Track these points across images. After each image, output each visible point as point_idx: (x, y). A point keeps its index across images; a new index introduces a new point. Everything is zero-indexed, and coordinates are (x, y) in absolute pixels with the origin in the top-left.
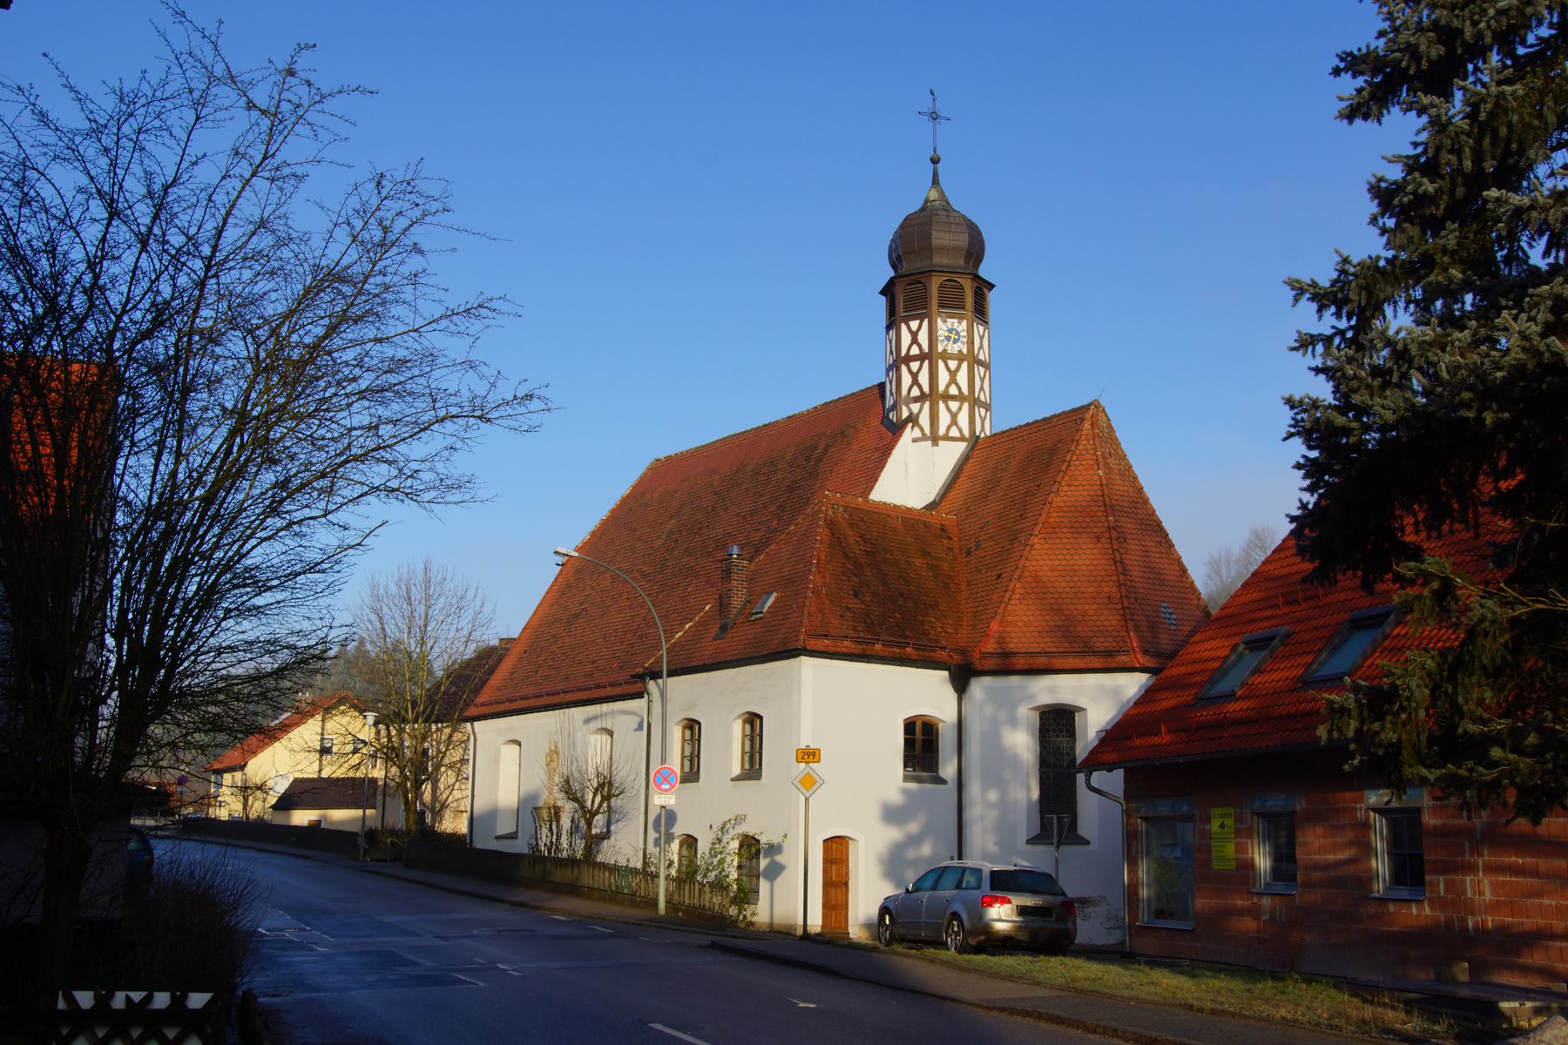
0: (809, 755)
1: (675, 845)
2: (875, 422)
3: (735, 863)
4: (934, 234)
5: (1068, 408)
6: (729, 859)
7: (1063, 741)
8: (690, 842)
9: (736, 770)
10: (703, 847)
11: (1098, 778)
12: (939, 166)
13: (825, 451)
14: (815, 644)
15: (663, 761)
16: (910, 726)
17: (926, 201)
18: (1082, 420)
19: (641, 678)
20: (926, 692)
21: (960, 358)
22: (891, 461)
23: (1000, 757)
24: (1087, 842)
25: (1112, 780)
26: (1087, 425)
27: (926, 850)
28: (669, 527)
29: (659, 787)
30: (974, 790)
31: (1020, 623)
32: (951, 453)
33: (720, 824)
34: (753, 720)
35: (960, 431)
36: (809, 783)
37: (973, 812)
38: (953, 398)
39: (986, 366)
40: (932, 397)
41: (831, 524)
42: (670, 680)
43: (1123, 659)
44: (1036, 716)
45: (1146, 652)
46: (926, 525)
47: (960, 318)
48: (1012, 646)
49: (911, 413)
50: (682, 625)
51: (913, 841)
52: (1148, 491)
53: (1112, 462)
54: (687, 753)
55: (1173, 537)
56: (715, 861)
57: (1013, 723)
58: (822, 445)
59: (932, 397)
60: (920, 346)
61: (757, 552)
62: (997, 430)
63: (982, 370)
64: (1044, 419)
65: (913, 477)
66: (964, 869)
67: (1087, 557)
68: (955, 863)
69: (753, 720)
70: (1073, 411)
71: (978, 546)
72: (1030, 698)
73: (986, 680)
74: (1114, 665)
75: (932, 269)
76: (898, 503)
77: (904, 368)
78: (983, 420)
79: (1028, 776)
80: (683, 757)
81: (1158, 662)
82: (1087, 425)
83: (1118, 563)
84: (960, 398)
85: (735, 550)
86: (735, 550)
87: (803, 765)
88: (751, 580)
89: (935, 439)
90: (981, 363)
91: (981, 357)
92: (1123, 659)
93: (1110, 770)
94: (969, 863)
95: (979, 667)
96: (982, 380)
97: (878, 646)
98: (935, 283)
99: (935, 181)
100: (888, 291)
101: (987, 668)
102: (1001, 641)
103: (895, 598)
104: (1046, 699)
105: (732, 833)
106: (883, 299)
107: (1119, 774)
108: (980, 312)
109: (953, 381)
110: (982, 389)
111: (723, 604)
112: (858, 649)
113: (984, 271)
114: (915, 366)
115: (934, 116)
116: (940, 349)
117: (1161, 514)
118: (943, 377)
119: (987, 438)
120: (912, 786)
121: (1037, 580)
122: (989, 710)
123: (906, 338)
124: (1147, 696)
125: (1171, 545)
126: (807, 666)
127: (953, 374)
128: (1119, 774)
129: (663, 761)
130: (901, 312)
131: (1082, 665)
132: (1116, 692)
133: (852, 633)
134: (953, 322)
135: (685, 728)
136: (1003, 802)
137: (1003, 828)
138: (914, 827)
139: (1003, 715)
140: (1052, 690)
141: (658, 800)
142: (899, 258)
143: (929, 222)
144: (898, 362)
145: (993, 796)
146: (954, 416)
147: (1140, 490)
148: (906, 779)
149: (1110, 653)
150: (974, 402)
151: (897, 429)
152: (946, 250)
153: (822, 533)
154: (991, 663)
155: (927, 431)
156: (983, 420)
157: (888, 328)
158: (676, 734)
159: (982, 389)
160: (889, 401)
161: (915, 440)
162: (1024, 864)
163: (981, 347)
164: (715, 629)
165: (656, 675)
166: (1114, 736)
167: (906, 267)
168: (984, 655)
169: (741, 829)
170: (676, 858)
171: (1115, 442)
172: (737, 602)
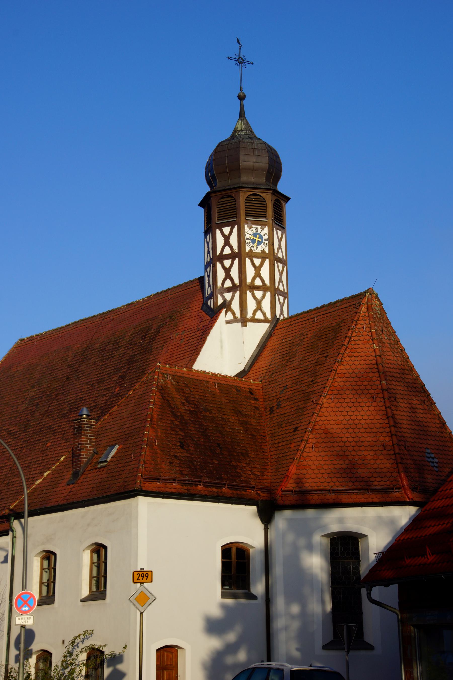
0: (143, 576)
1: (33, 661)
2: (197, 307)
3: (83, 673)
4: (241, 157)
5: (348, 295)
6: (78, 669)
7: (246, 370)
8: (45, 656)
9: (85, 592)
10: (57, 660)
11: (376, 592)
12: (245, 102)
13: (158, 332)
14: (148, 486)
15: (24, 587)
16: (226, 551)
17: (235, 131)
18: (360, 304)
19: (7, 518)
20: (240, 524)
21: (263, 256)
22: (209, 338)
23: (299, 577)
24: (371, 648)
25: (388, 594)
26: (364, 309)
27: (242, 656)
28: (31, 394)
29: (19, 609)
30: (279, 603)
31: (313, 466)
32: (257, 332)
33: (71, 639)
34: (99, 550)
35: (264, 314)
36: (144, 600)
37: (279, 623)
38: (258, 288)
39: (284, 262)
40: (241, 287)
41: (162, 390)
42: (31, 519)
43: (396, 495)
44: (326, 542)
45: (413, 489)
46: (238, 390)
47: (263, 225)
48: (307, 485)
49: (225, 300)
50: (42, 473)
51: (231, 649)
52: (413, 360)
53: (384, 337)
54: (45, 579)
55: (434, 396)
56: (67, 671)
57: (310, 548)
58: (155, 326)
59: (241, 287)
60: (231, 247)
61: (103, 413)
62: (293, 313)
63: (281, 266)
64: (330, 304)
65: (227, 351)
66: (270, 669)
67: (366, 413)
68: (265, 664)
69: (99, 550)
70: (353, 297)
71: (279, 406)
72: (324, 527)
73: (288, 513)
74: (389, 500)
75: (240, 185)
76: (216, 372)
77: (219, 265)
78: (282, 306)
79: (322, 592)
80: (41, 583)
81: (422, 495)
82: (364, 309)
83: (390, 418)
84: (263, 288)
85: (85, 411)
86: (85, 411)
87: (139, 585)
88: (97, 435)
89: (244, 321)
90: (280, 260)
91: (280, 255)
92: (396, 495)
93: (386, 586)
94: (274, 664)
95: (281, 502)
96: (281, 274)
97: (200, 487)
98: (243, 196)
99: (242, 115)
100: (205, 203)
101: (287, 503)
102: (299, 481)
103: (211, 446)
104: (335, 528)
105: (81, 646)
106: (202, 210)
107: (394, 588)
108: (279, 220)
109: (258, 274)
110: (281, 281)
111: (75, 456)
112: (184, 489)
113: (281, 187)
114: (227, 263)
115: (240, 61)
116: (247, 249)
117: (424, 378)
118: (250, 272)
119: (285, 319)
120: (229, 601)
121: (326, 432)
122: (290, 538)
123: (220, 241)
124: (415, 523)
125: (432, 403)
126: (143, 502)
127: (258, 269)
128: (394, 588)
129: (24, 587)
130: (216, 220)
131: (363, 500)
132: (392, 522)
133: (178, 477)
134: (257, 228)
135: (43, 558)
136: (304, 615)
137: (304, 635)
138: (231, 637)
139: (302, 542)
140: (341, 520)
141: (18, 621)
142: (213, 177)
143: (238, 148)
144: (211, 264)
145: (295, 609)
146: (259, 303)
147: (407, 359)
148: (224, 595)
149: (386, 490)
150: (275, 292)
151: (214, 314)
152: (251, 170)
153: (154, 396)
154: (291, 499)
155: (238, 315)
156: (282, 306)
157: (206, 233)
158: (36, 564)
159: (281, 281)
160: (208, 291)
161: (228, 322)
162: (318, 665)
163: (280, 247)
164: (69, 475)
165: (19, 516)
166: (388, 556)
167: (219, 185)
168: (286, 493)
169: (89, 643)
170: (33, 671)
171: (385, 321)
172: (86, 453)
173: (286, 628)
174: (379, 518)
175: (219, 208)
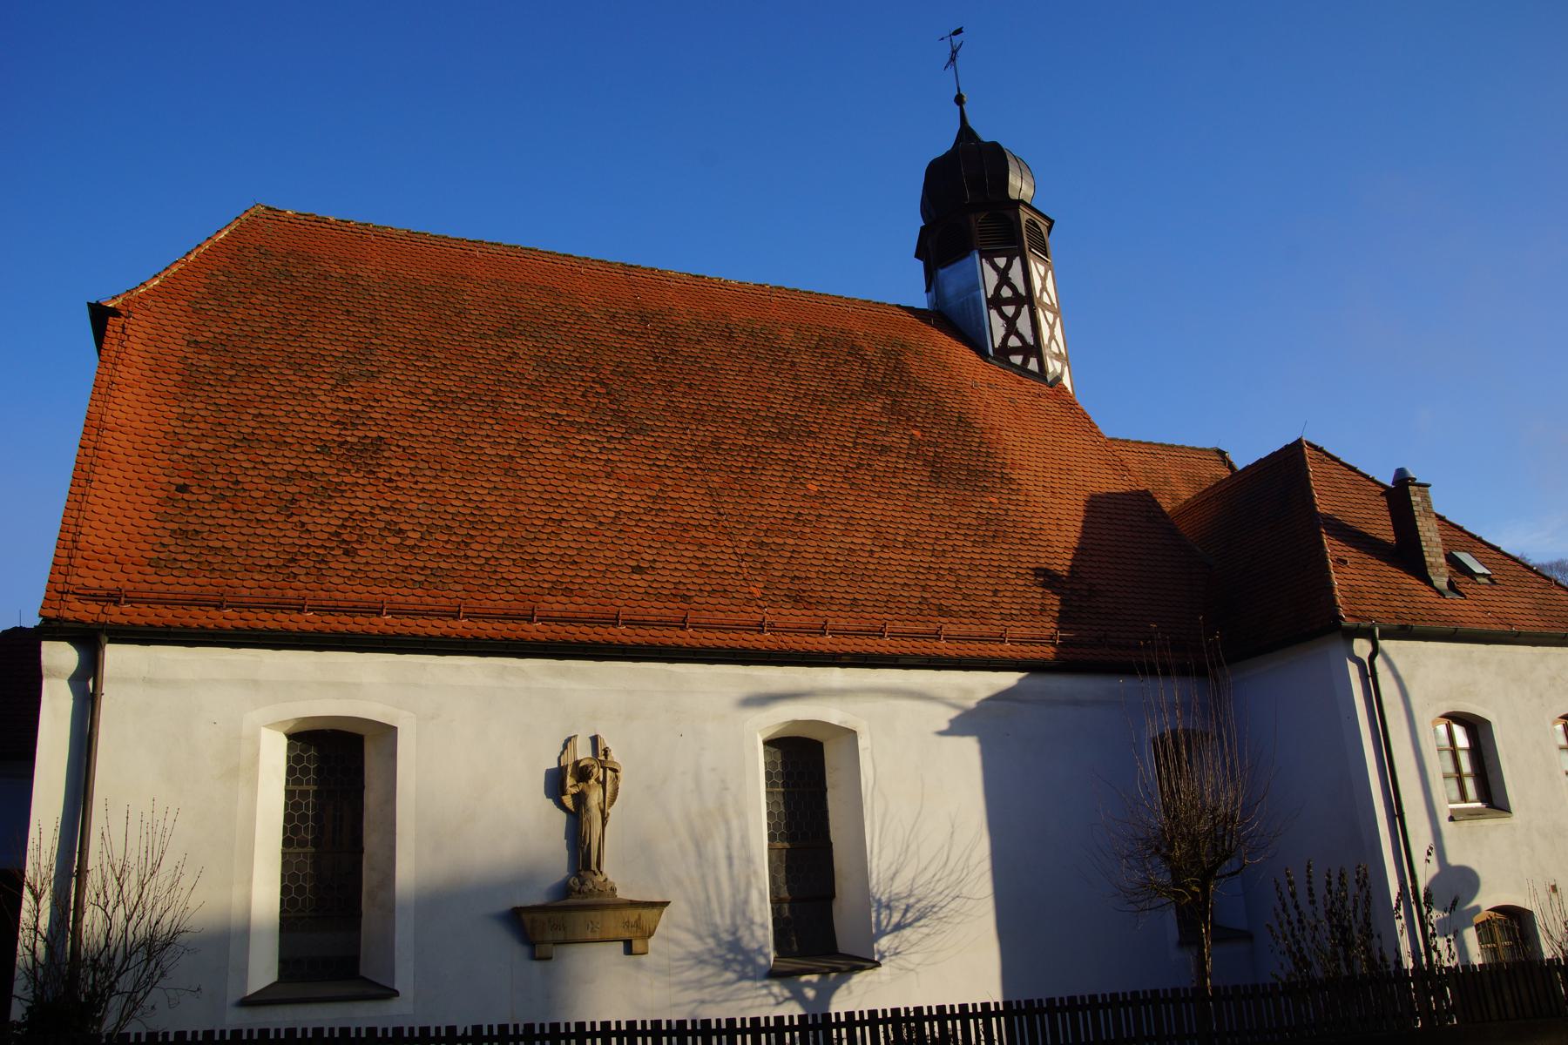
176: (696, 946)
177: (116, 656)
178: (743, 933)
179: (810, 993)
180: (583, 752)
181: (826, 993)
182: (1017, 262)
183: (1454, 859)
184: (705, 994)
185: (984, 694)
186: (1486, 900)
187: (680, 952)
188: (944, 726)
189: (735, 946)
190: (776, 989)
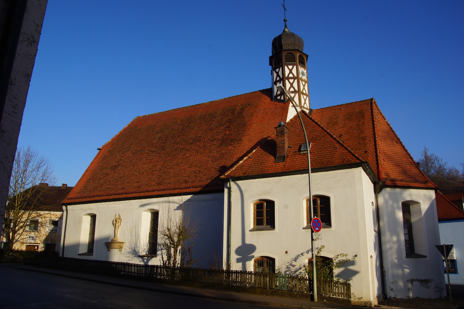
73: (388, 190)
122: (390, 203)
173: (391, 248)
174: (425, 195)
175: (277, 61)
176: (129, 250)
177: (69, 207)
178: (136, 248)
179: (145, 261)
180: (117, 217)
181: (148, 261)
182: (295, 67)
183: (248, 242)
184: (129, 259)
185: (184, 201)
186: (257, 254)
187: (126, 251)
188: (176, 208)
189: (134, 251)
190: (140, 259)
